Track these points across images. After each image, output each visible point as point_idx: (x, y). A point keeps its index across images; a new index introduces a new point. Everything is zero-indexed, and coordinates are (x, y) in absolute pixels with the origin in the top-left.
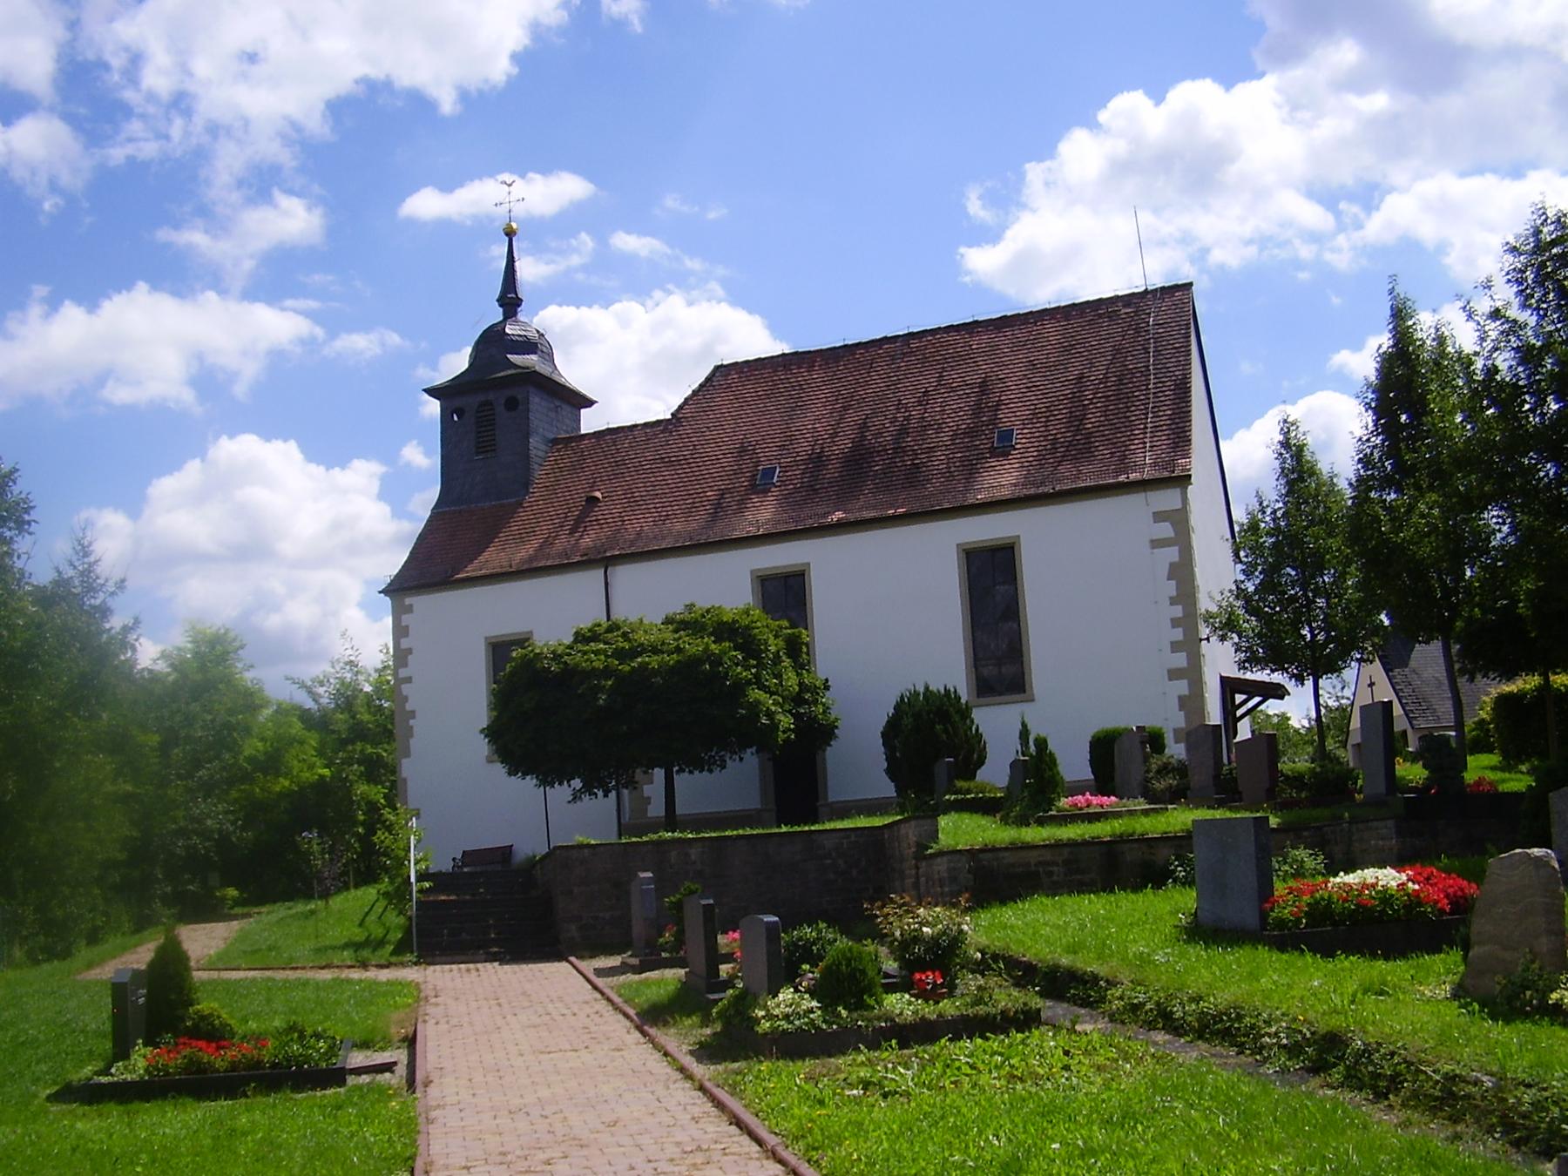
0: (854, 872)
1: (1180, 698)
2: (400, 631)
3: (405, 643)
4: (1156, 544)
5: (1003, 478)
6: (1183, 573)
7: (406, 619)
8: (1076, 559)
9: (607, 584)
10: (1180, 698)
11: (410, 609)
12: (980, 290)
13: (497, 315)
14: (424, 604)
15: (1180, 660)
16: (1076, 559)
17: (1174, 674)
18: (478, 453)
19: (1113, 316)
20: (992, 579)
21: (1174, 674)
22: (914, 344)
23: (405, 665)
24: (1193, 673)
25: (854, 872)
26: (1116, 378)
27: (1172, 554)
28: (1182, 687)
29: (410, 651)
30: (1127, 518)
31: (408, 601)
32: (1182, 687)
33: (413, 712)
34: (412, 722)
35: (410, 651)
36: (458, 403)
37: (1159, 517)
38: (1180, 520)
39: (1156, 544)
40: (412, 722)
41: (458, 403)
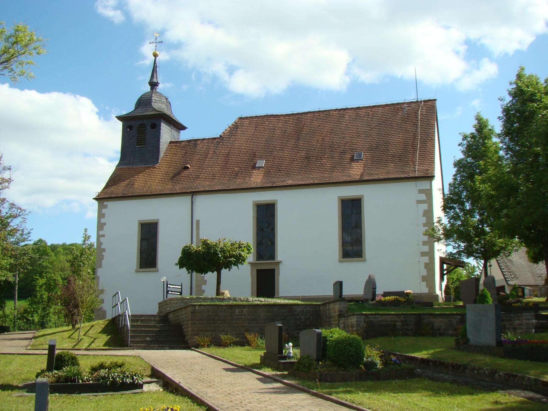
0: (308, 322)
1: (425, 264)
2: (101, 215)
3: (103, 221)
4: (419, 202)
5: (356, 170)
6: (429, 213)
7: (104, 211)
8: (383, 205)
9: (192, 202)
10: (425, 264)
11: (106, 207)
12: (239, 97)
13: (148, 88)
14: (111, 205)
15: (426, 249)
16: (383, 205)
17: (423, 254)
18: (138, 145)
19: (402, 109)
20: (266, 216)
21: (423, 254)
22: (322, 115)
23: (102, 229)
24: (431, 254)
25: (308, 322)
26: (395, 134)
27: (425, 206)
28: (426, 259)
29: (105, 224)
30: (408, 191)
31: (105, 203)
32: (426, 259)
33: (105, 249)
34: (103, 253)
35: (105, 224)
36: (131, 123)
37: (421, 191)
38: (429, 193)
39: (419, 202)
40: (103, 253)
41: (131, 123)
